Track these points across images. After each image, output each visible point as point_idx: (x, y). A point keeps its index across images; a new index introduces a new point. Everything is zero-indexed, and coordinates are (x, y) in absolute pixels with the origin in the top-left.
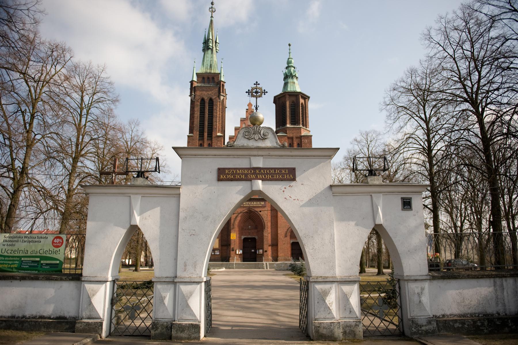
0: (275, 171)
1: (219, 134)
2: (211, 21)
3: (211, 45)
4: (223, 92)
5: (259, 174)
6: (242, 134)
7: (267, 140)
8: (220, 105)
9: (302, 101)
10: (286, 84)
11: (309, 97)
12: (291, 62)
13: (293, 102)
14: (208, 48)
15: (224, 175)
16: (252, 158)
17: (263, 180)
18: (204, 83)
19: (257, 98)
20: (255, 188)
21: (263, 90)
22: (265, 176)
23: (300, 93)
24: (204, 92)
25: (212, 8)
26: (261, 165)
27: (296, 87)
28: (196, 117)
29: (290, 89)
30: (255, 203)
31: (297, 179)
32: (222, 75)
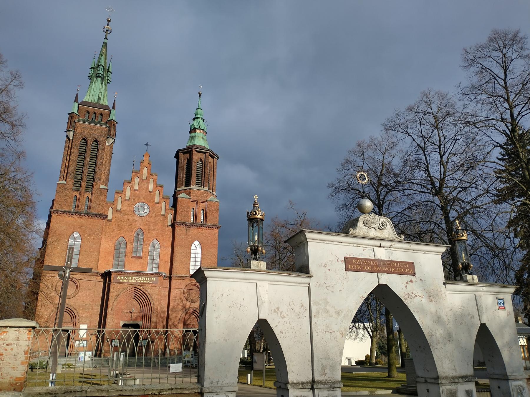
0: (397, 264)
1: (102, 186)
2: (105, 44)
15: (352, 264)
22: (389, 269)
30: (143, 279)
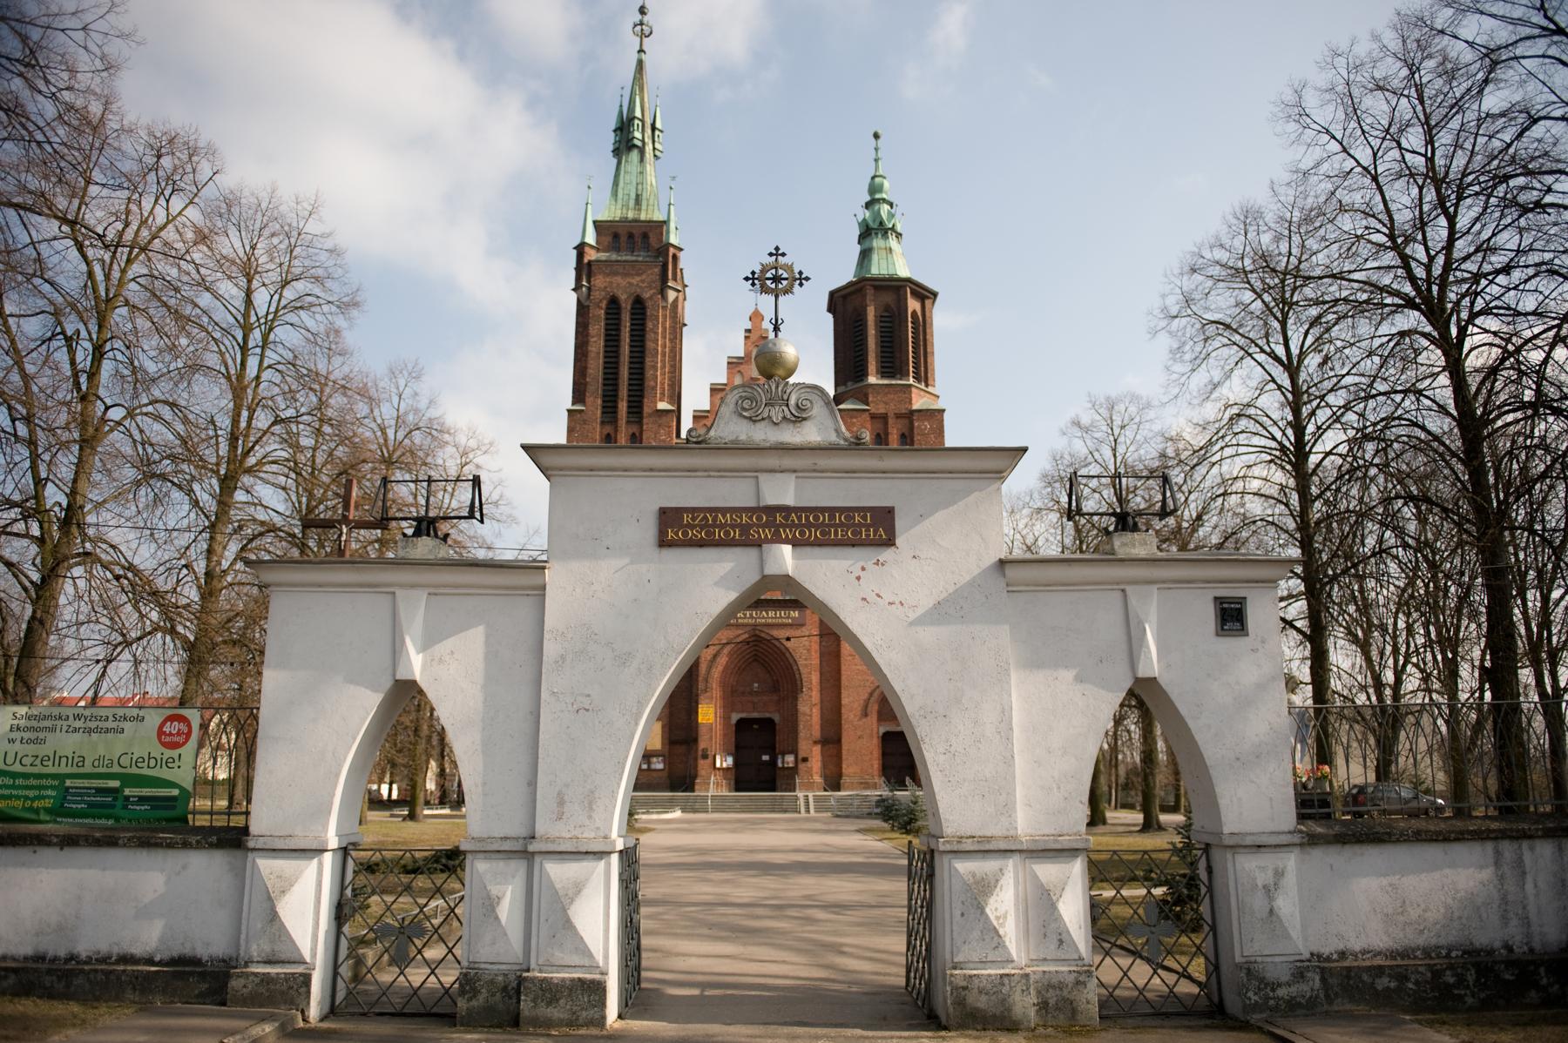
0: (832, 517)
1: (662, 405)
2: (640, 63)
3: (638, 135)
4: (675, 279)
5: (784, 526)
6: (732, 406)
7: (807, 424)
8: (665, 317)
9: (913, 305)
10: (865, 255)
11: (935, 295)
12: (880, 189)
13: (887, 308)
14: (630, 146)
15: (679, 530)
16: (763, 477)
17: (795, 544)
18: (618, 250)
19: (777, 297)
20: (771, 570)
21: (796, 271)
22: (802, 533)
23: (909, 280)
24: (619, 279)
25: (641, 24)
26: (789, 500)
27: (897, 262)
28: (592, 355)
29: (878, 268)
30: (771, 614)
31: (898, 542)
32: (672, 225)
